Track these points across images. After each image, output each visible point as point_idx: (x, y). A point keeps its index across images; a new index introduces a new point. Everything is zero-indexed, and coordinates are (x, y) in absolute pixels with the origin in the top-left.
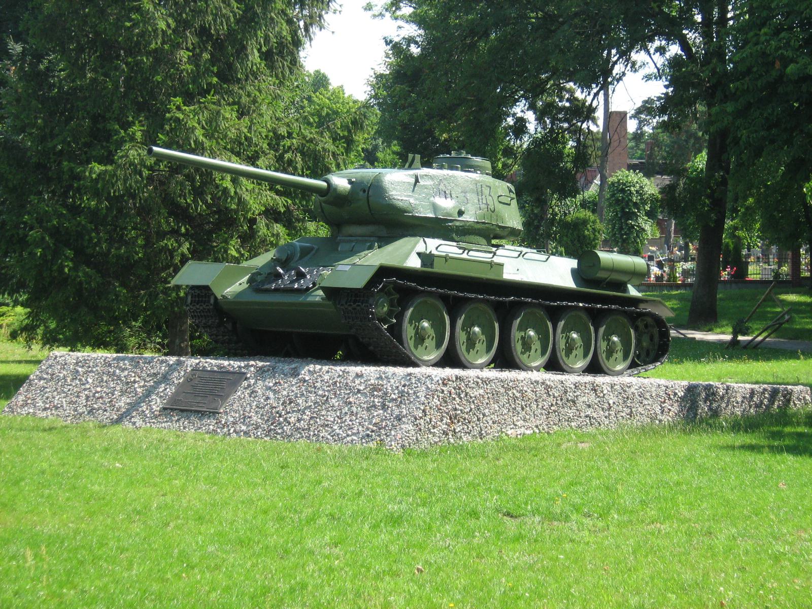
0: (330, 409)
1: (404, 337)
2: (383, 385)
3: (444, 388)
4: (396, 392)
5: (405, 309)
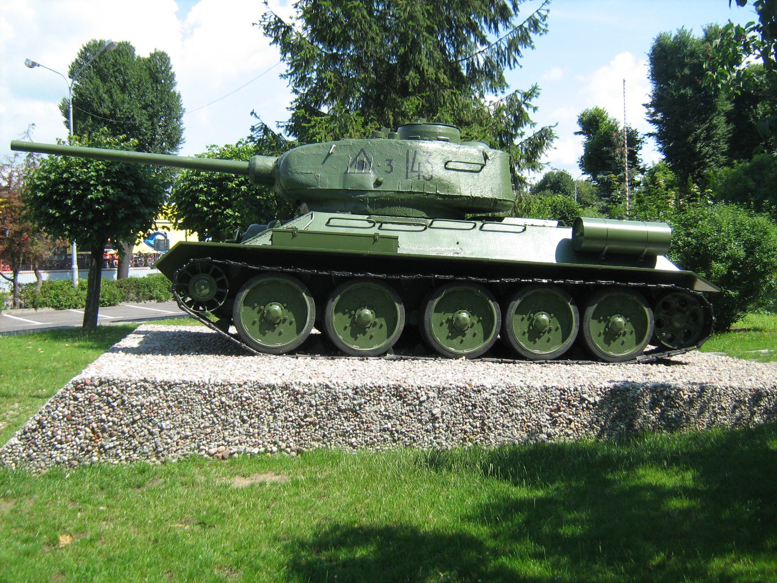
3: (79, 395)
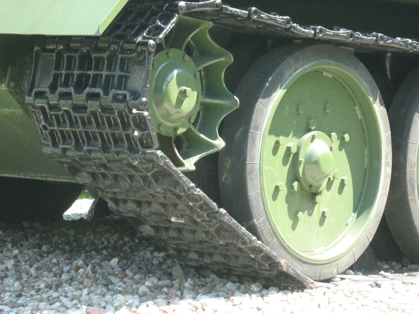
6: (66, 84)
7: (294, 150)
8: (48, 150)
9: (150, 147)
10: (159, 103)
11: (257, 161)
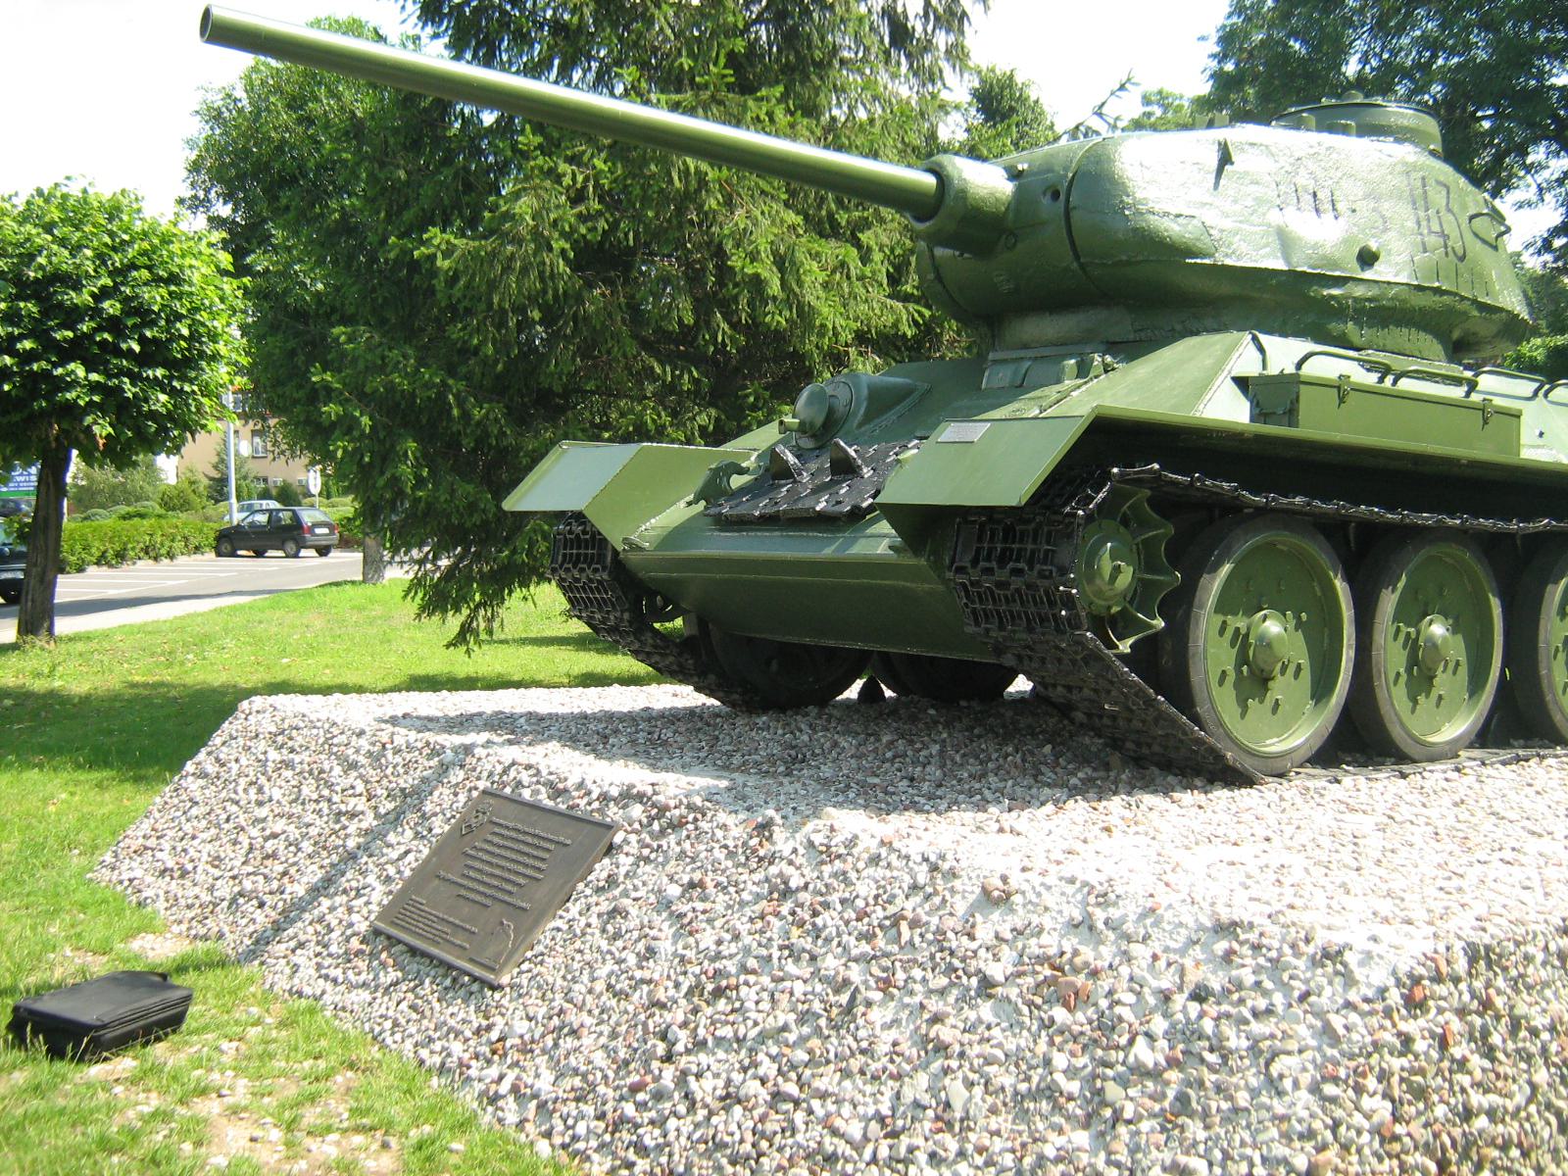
0: (855, 1064)
1: (1196, 678)
2: (1094, 974)
4: (1159, 1025)
5: (1196, 570)
6: (988, 559)
7: (1243, 631)
8: (970, 629)
9: (1079, 628)
10: (1091, 580)
11: (1201, 643)
